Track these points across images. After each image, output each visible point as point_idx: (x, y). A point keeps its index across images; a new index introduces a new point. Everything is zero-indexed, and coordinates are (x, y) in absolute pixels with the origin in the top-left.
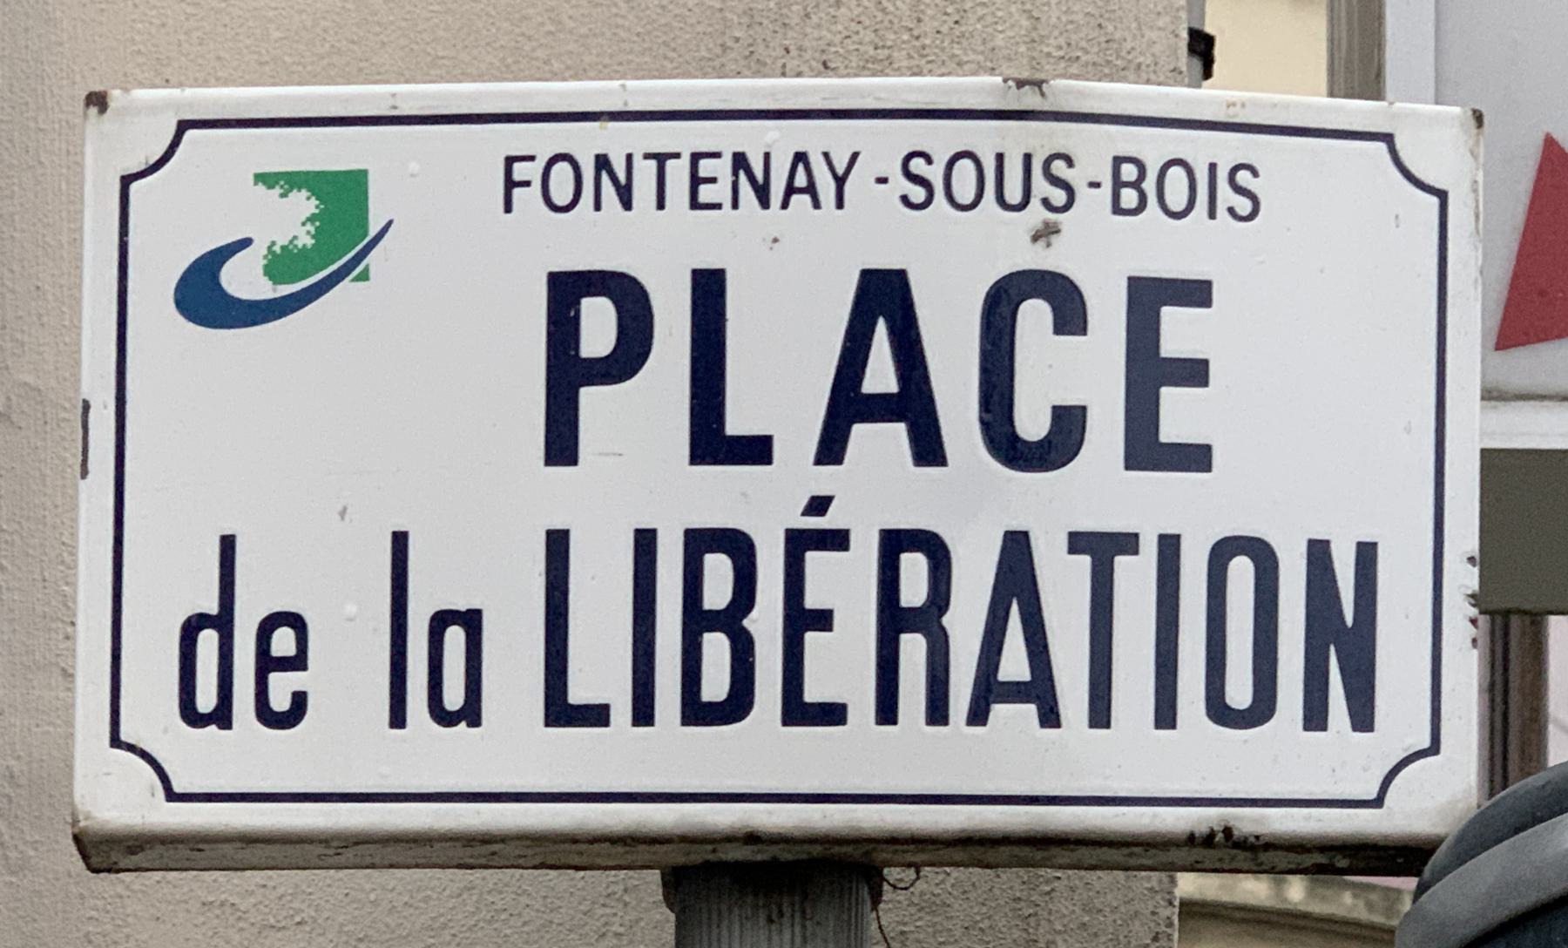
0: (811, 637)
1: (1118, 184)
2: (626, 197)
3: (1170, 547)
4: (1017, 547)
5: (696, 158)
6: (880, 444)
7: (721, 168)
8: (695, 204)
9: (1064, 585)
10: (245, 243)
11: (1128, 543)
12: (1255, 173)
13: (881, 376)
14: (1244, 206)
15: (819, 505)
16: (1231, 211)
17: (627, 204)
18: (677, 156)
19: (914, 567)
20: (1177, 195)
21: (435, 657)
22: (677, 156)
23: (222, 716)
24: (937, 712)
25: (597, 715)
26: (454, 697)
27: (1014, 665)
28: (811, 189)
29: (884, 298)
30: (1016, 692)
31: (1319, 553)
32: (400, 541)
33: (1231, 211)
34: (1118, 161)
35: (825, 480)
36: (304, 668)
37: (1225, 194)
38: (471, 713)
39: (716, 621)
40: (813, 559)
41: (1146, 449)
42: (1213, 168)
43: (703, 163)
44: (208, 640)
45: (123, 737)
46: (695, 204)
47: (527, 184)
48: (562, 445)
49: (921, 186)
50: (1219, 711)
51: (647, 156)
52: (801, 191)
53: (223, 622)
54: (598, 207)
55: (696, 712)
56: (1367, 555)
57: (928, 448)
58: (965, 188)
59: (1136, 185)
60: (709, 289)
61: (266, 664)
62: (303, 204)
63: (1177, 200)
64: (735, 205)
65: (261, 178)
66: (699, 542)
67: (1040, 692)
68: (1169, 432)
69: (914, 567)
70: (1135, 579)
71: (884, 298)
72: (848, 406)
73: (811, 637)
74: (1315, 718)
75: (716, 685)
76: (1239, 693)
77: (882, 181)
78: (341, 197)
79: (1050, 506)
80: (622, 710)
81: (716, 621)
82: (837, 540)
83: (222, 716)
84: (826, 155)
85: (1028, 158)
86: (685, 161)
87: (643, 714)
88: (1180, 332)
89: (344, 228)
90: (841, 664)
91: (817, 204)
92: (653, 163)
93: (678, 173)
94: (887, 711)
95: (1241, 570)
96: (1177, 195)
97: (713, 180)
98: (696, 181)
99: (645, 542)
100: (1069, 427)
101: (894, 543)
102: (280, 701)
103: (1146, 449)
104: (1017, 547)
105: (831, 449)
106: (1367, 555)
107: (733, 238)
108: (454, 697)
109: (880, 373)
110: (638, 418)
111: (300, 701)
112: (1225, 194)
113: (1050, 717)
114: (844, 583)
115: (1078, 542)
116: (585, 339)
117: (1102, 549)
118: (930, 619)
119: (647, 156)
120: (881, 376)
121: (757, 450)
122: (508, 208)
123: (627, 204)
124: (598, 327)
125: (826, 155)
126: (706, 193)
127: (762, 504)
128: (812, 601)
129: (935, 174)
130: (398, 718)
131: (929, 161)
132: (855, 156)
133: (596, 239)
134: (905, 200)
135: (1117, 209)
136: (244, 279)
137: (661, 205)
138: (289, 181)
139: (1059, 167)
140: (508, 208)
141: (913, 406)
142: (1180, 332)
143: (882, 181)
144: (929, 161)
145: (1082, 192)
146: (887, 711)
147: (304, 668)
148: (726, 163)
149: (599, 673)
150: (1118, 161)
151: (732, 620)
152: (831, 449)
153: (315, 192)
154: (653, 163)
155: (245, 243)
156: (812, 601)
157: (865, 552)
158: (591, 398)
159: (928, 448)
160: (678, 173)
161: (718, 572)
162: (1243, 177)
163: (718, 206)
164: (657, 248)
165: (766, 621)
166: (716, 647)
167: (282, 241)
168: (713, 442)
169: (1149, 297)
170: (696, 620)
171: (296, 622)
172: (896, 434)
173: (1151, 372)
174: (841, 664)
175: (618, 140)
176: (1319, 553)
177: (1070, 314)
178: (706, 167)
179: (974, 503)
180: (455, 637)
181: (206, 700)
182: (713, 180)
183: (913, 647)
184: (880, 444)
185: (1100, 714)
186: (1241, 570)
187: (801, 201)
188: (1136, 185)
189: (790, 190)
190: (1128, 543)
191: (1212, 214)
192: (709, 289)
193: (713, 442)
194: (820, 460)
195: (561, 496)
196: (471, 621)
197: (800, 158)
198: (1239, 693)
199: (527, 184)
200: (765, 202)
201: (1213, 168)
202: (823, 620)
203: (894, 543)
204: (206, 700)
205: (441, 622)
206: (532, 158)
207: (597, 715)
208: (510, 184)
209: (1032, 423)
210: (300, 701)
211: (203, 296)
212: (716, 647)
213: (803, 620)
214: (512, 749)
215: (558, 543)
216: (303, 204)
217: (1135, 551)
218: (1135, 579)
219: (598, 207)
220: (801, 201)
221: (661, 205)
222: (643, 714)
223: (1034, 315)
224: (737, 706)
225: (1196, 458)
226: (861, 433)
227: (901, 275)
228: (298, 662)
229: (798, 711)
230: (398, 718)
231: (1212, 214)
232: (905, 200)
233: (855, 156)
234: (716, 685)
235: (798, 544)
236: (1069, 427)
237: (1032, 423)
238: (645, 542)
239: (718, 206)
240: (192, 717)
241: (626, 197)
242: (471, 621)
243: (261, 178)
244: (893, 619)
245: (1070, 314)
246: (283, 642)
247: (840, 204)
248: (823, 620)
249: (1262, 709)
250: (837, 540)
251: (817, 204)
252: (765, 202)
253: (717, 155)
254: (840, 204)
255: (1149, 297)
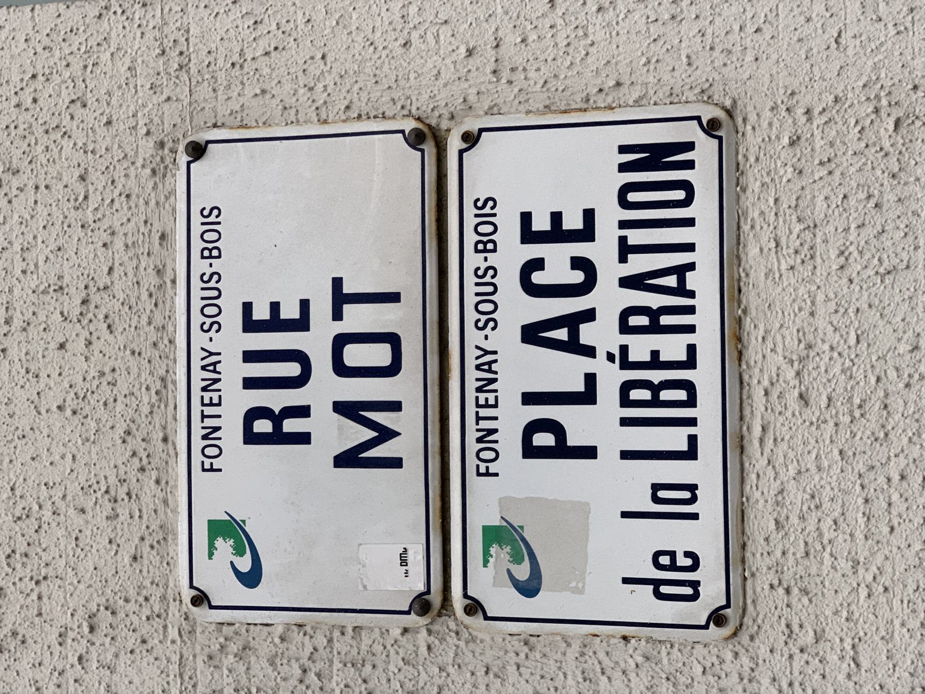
0: (663, 358)
1: (211, 257)
2: (217, 429)
3: (623, 225)
4: (627, 282)
5: (203, 404)
6: (587, 334)
7: (482, 397)
8: (219, 404)
9: (639, 264)
10: (509, 571)
11: (623, 240)
12: (204, 209)
13: (562, 334)
14: (215, 212)
15: (611, 357)
16: (217, 217)
17: (496, 431)
18: (202, 411)
19: (634, 321)
20: (489, 229)
21: (673, 502)
22: (202, 411)
23: (695, 585)
24: (691, 310)
25: (692, 440)
26: (687, 495)
27: (671, 281)
28: (490, 363)
29: (532, 334)
30: (682, 281)
31: (623, 168)
32: (625, 515)
33: (217, 217)
34: (203, 257)
35: (601, 354)
36: (675, 552)
37: (487, 210)
38: (692, 488)
39: (656, 395)
40: (632, 358)
41: (587, 234)
42: (203, 224)
43: (480, 403)
44: (664, 589)
45: (703, 623)
46: (219, 404)
47: (212, 464)
48: (589, 452)
49: (489, 322)
50: (687, 202)
51: (203, 422)
52: (215, 368)
53: (656, 583)
54: (220, 439)
55: (691, 402)
56: (623, 149)
57: (589, 315)
58: (489, 307)
59: (210, 250)
60: (529, 399)
61: (673, 567)
62: (219, 542)
63: (490, 229)
64: (220, 390)
65: (210, 557)
66: (625, 402)
67: (681, 271)
68: (579, 225)
69: (634, 321)
70: (636, 237)
71: (532, 334)
72: (574, 346)
73: (663, 358)
74: (690, 165)
75: (681, 395)
76: (680, 195)
77: (211, 339)
78: (217, 529)
79: (610, 269)
80: (691, 430)
81: (656, 395)
82: (624, 349)
83: (695, 585)
84: (202, 359)
85: (203, 289)
86: (204, 408)
87: (692, 422)
88: (541, 223)
89: (226, 528)
90: (673, 347)
91: (219, 362)
92: (205, 420)
93: (208, 411)
94: (691, 329)
95: (632, 197)
96: (489, 229)
97: (211, 398)
98: (211, 404)
99: (625, 422)
100: (578, 263)
101: (625, 328)
102: (689, 562)
103: (587, 234)
104: (627, 282)
105: (590, 352)
106: (623, 149)
107: (509, 389)
108: (687, 495)
109: (558, 334)
110: (578, 424)
111: (688, 554)
112: (487, 210)
113: (691, 267)
114: (641, 347)
115: (623, 259)
116: (549, 443)
117: (625, 250)
118: (654, 314)
119: (203, 422)
120: (562, 334)
121: (590, 379)
122: (220, 470)
123: (496, 431)
124: (544, 439)
125: (202, 359)
126: (492, 401)
127: (611, 379)
128: (647, 358)
129: (484, 318)
130: (695, 516)
131: (204, 323)
132: (202, 349)
133: (509, 440)
134: (217, 331)
135: (219, 257)
136: (523, 572)
137: (219, 416)
138: (486, 555)
139: (480, 273)
140: (220, 470)
141: (573, 321)
142: (541, 223)
143: (211, 339)
144: (204, 323)
145: (213, 270)
146: (691, 329)
147: (675, 552)
148: (204, 394)
149: (676, 439)
150: (203, 257)
151: (655, 389)
152: (590, 352)
153: (490, 546)
154: (205, 420)
155: (509, 571)
156: (647, 358)
157: (627, 339)
158: (572, 441)
159: (589, 315)
160: (208, 411)
161: (635, 395)
162: (206, 213)
163: (220, 397)
164: (512, 418)
165: (656, 376)
166: (665, 395)
167: (508, 557)
168: (588, 396)
169: (529, 236)
170: (655, 402)
171: (657, 555)
172: (583, 328)
173: (558, 233)
174: (673, 347)
175: (198, 432)
176: (623, 168)
177: (537, 264)
178: (207, 401)
179: (609, 299)
180: (662, 494)
181: (689, 591)
182: (211, 398)
183: (665, 320)
184: (587, 334)
185: (690, 248)
186: (632, 197)
187: (494, 367)
188: (210, 250)
189: (215, 371)
190: (623, 240)
191: (219, 223)
192: (529, 399)
193: (588, 396)
194: (594, 356)
195: (608, 454)
196: (656, 487)
197: (203, 368)
198: (680, 195)
199: (212, 464)
200: (219, 380)
201: (203, 224)
202: (655, 354)
203: (625, 328)
204: (689, 591)
205: (656, 500)
206: (203, 462)
207: (692, 440)
208: (211, 470)
209: (578, 277)
210: (688, 554)
211: (251, 578)
212: (665, 395)
213: (655, 362)
214: (705, 472)
215: (626, 455)
216: (219, 542)
217: (626, 237)
218: (636, 237)
219: (220, 439)
220: (494, 367)
221: (219, 416)
222: (692, 422)
223: (537, 278)
224: (688, 386)
225: (589, 215)
226: (584, 340)
227: (523, 327)
228: (672, 554)
229: (690, 362)
230: (695, 516)
231: (219, 223)
232: (217, 331)
233: (202, 349)
234: (681, 395)
235: (626, 364)
236: (578, 263)
237: (578, 277)
238: (625, 422)
239: (220, 397)
240: (695, 597)
241: (217, 429)
242: (656, 487)
243: (210, 557)
244: (655, 328)
245: (537, 264)
246: (665, 560)
247: (219, 354)
248: (655, 354)
249: (687, 186)
250: (624, 349)
251: (219, 362)
252: (495, 380)
253: (202, 397)
254: (219, 354)
255: (529, 236)
